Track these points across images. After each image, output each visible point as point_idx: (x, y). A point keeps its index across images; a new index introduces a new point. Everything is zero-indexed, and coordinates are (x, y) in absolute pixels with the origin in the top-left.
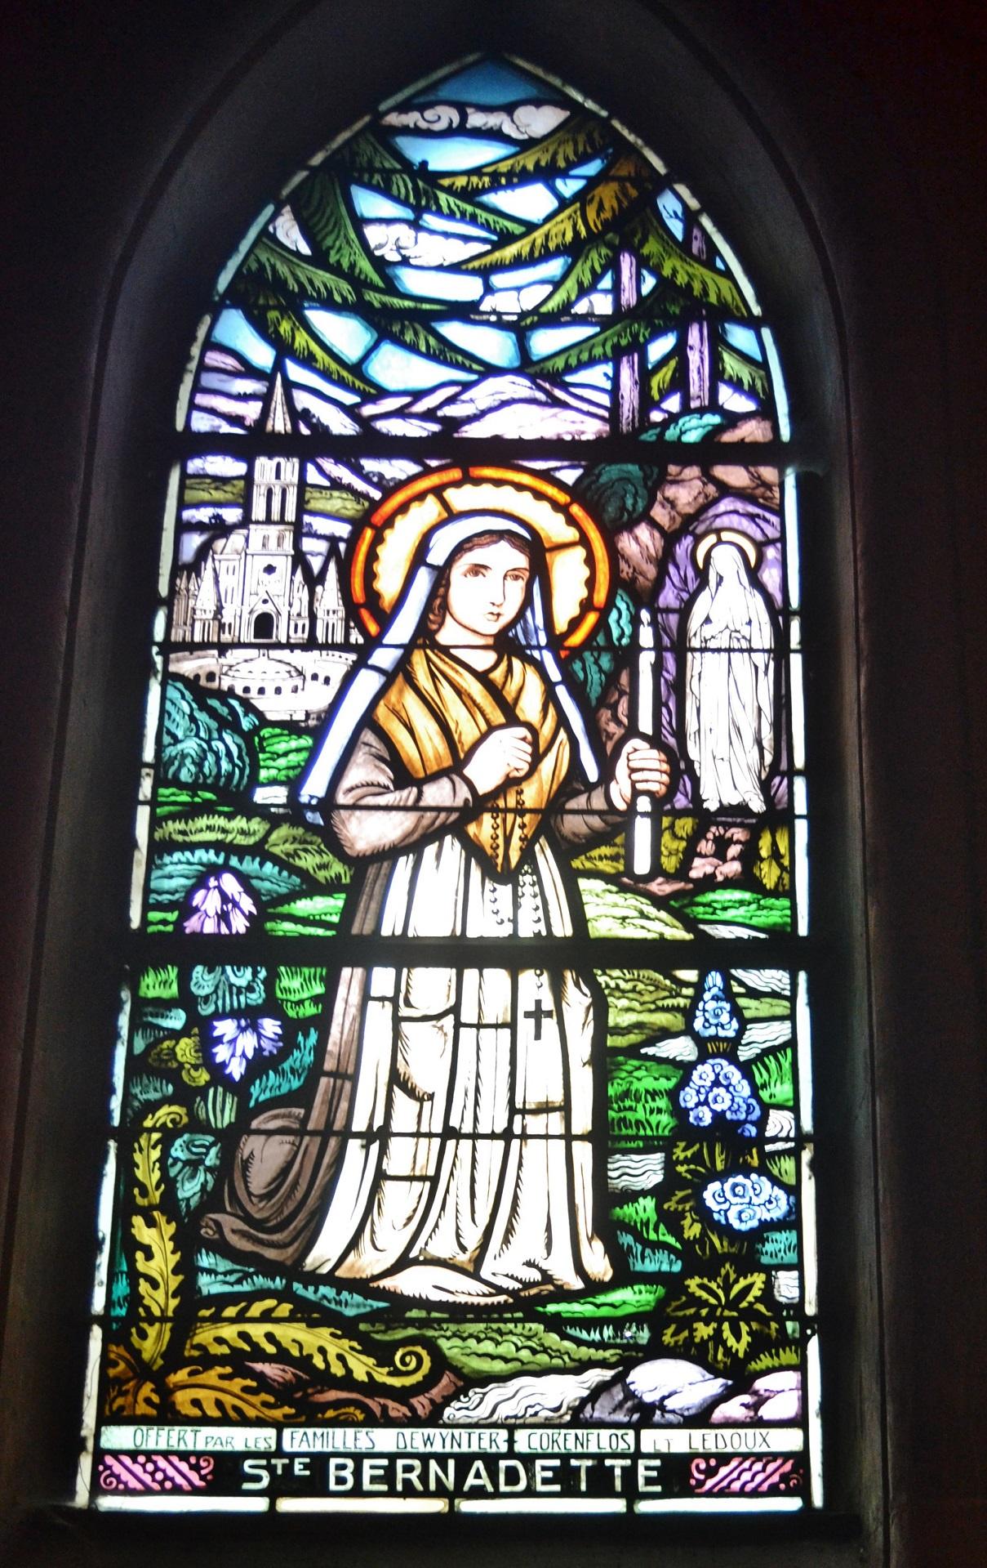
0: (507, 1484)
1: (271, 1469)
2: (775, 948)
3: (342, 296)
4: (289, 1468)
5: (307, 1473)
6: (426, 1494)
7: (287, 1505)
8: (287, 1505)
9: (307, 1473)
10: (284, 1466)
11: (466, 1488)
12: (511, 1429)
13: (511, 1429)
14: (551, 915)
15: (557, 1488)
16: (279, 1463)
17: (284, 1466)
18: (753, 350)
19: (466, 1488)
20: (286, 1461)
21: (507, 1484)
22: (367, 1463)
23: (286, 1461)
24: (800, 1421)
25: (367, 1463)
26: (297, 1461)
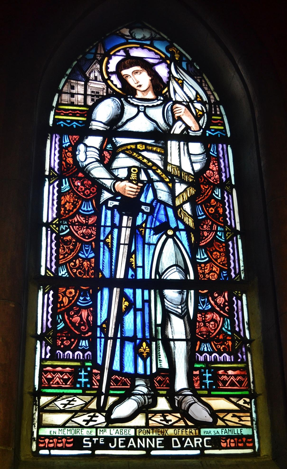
0: (175, 445)
1: (92, 441)
2: (199, 322)
3: (143, 217)
4: (98, 441)
5: (103, 443)
6: (137, 449)
7: (98, 452)
8: (98, 452)
9: (103, 443)
10: (96, 440)
11: (185, 446)
12: (97, 428)
13: (97, 428)
14: (41, 313)
15: (163, 447)
16: (95, 439)
17: (96, 440)
18: (220, 235)
19: (185, 446)
20: (97, 439)
21: (175, 445)
22: (120, 439)
23: (97, 439)
24: (251, 427)
25: (120, 439)
26: (100, 439)
